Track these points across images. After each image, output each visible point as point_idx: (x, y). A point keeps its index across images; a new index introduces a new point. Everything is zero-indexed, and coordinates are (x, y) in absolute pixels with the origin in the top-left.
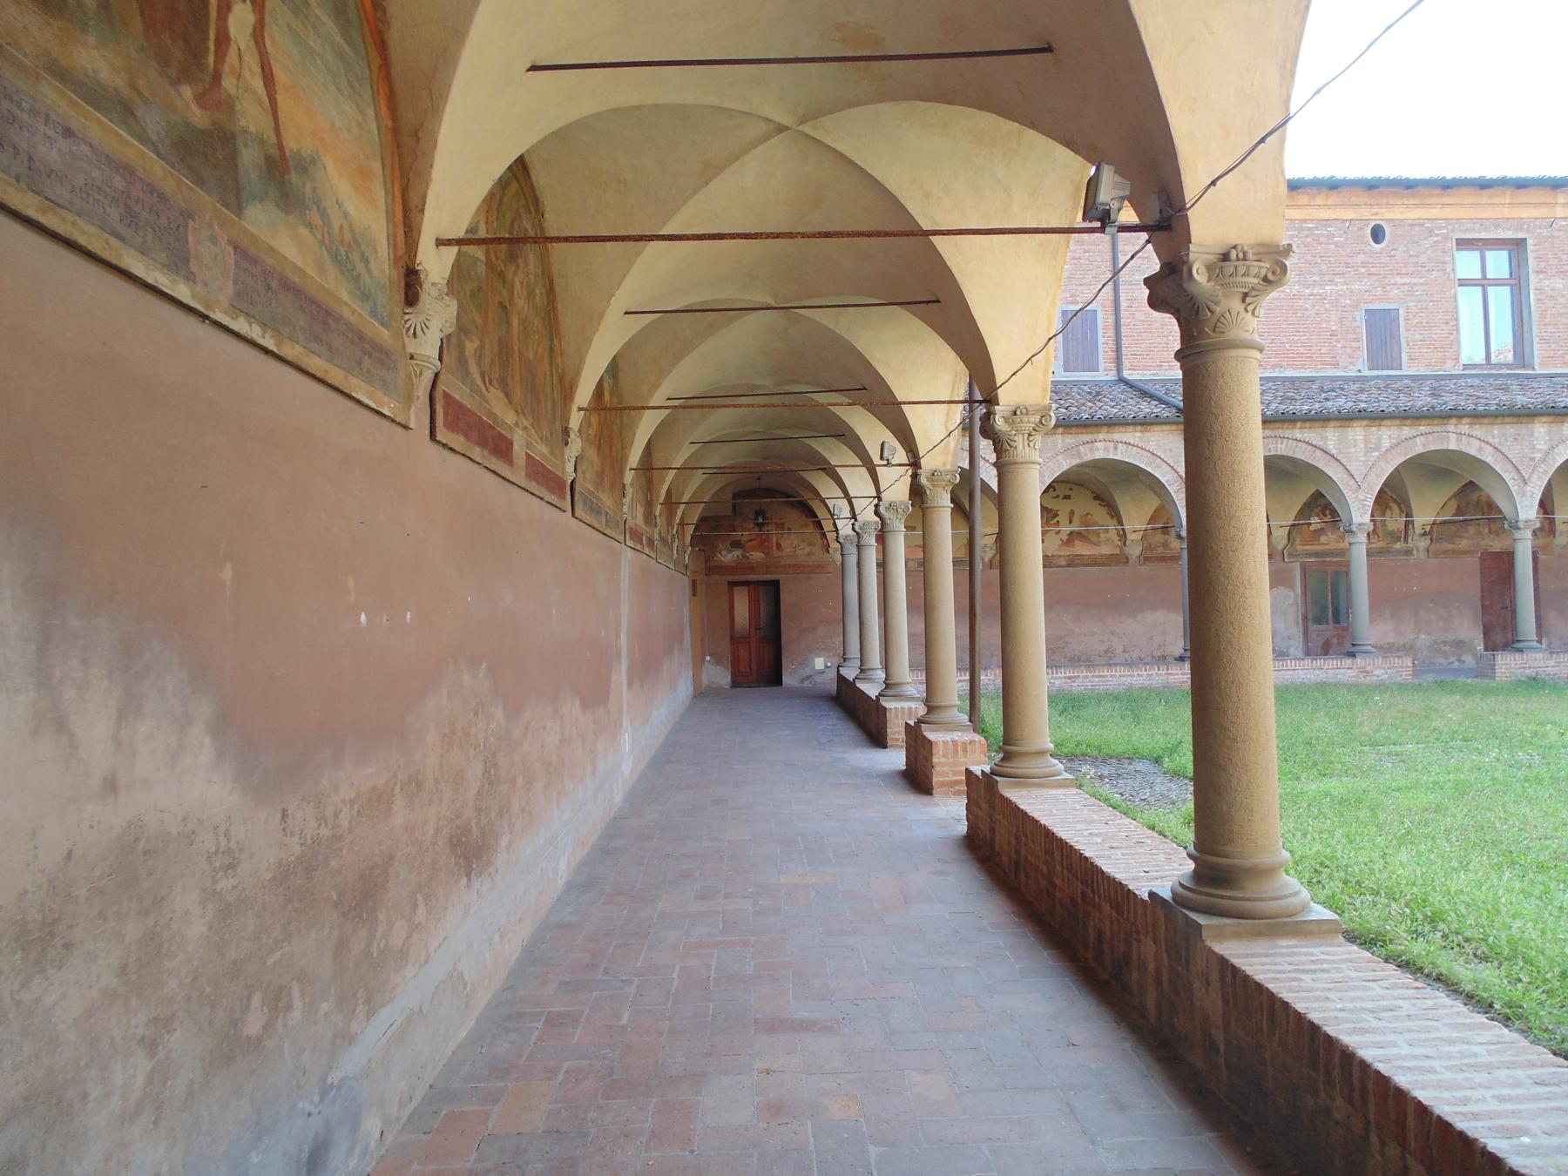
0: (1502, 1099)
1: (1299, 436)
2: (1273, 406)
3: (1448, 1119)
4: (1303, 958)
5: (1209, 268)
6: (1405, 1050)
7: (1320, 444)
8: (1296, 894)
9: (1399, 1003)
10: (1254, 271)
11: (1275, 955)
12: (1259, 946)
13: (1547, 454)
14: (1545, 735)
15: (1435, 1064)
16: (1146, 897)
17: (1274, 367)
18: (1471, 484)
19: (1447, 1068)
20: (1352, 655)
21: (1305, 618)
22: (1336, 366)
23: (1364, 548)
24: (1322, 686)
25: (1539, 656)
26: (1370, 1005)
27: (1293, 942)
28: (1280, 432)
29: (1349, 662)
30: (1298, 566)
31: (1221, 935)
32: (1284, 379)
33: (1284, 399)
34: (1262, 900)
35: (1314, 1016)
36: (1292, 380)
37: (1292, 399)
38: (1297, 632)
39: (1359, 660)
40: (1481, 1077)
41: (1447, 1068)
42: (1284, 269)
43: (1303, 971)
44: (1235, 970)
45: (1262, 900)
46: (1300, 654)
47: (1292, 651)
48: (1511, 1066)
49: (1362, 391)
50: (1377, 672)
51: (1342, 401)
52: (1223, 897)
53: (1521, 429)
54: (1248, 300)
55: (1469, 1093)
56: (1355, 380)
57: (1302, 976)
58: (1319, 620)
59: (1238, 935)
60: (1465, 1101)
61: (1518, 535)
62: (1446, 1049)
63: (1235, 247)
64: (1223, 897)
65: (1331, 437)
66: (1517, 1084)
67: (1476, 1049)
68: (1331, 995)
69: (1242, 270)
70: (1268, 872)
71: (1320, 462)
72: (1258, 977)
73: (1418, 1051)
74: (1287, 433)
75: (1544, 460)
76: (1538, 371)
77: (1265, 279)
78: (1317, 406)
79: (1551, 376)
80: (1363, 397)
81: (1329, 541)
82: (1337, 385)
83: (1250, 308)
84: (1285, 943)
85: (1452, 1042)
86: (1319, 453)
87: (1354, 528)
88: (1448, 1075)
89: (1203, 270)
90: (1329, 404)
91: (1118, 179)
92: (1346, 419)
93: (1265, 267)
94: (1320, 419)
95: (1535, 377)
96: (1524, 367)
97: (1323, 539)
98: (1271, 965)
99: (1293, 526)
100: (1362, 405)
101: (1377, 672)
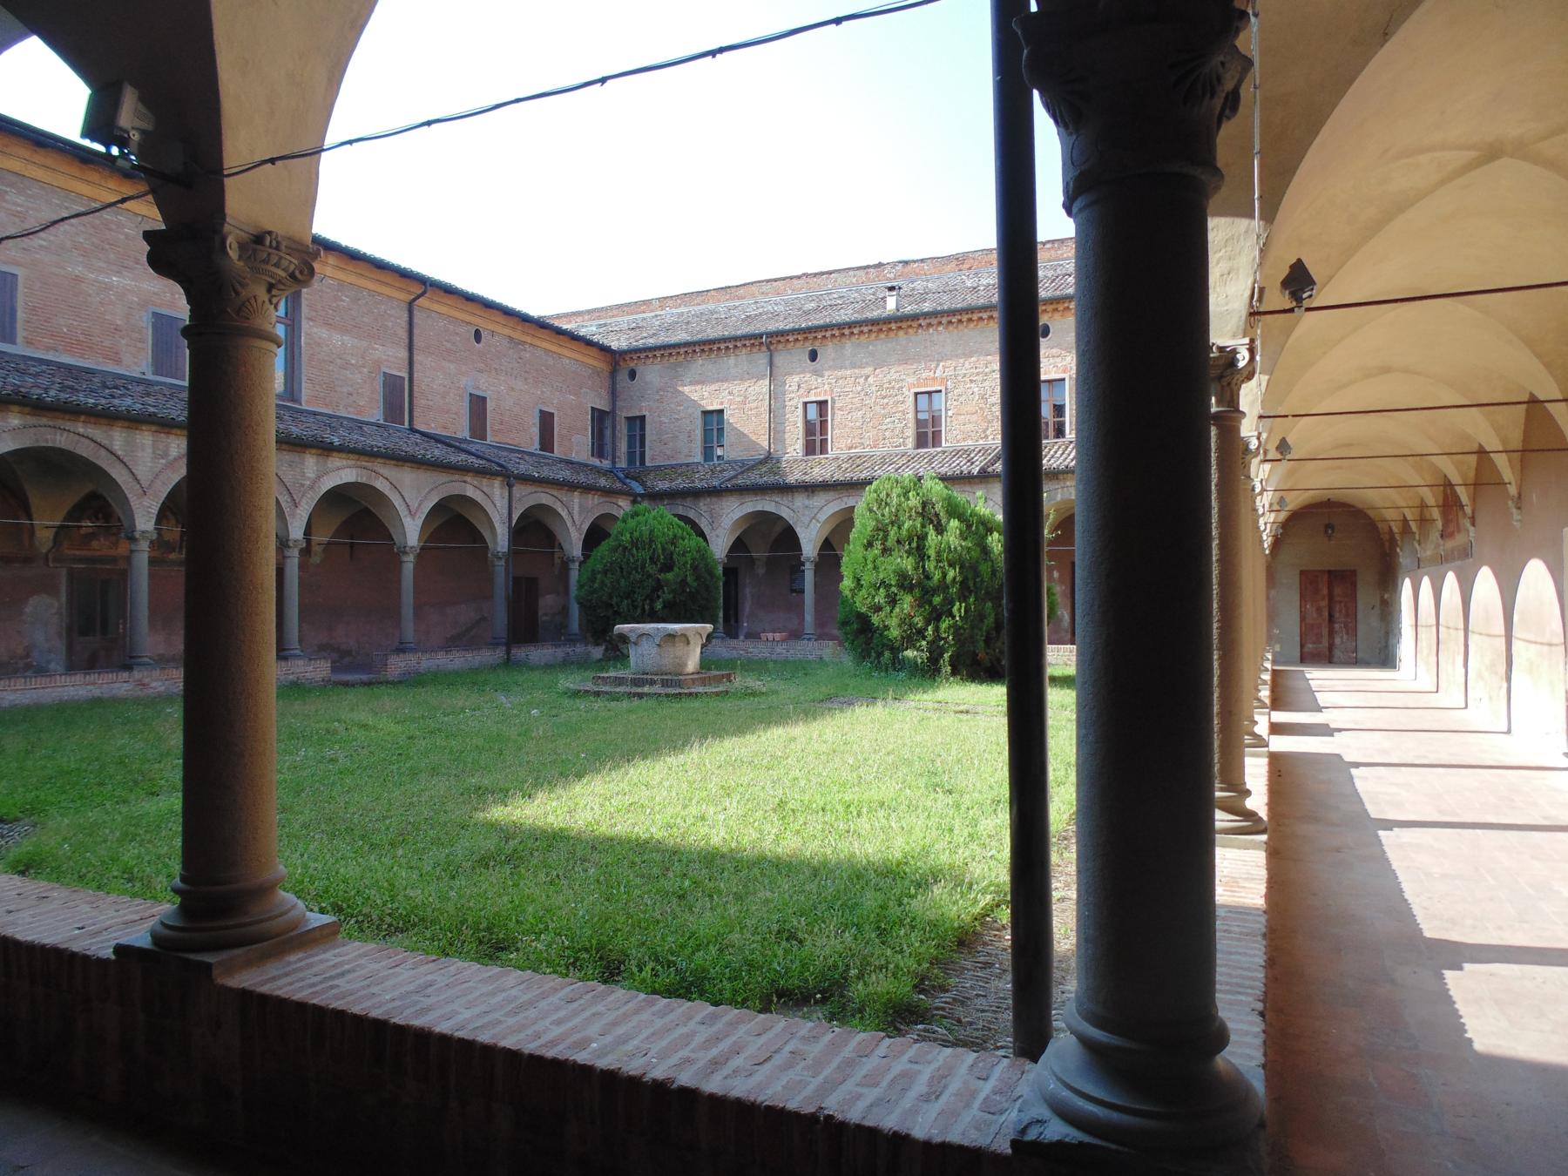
0: (558, 1023)
1: (81, 430)
2: (52, 393)
3: (538, 1053)
4: (322, 967)
5: (242, 247)
6: (467, 1014)
7: (105, 442)
8: (294, 907)
9: (429, 978)
10: (284, 263)
11: (295, 971)
12: (272, 969)
13: (314, 482)
14: (335, 732)
15: (497, 1015)
16: (108, 953)
17: (48, 349)
18: (367, 512)
19: (507, 1015)
20: (128, 668)
21: (70, 630)
22: (119, 362)
23: (146, 555)
24: (97, 702)
25: (301, 663)
26: (411, 987)
27: (300, 955)
28: (59, 423)
29: (125, 675)
30: (64, 572)
31: (231, 969)
32: (60, 366)
33: (63, 389)
34: (270, 919)
35: (375, 1013)
36: (69, 368)
37: (72, 388)
38: (60, 645)
39: (137, 674)
40: (532, 1013)
41: (507, 1015)
42: (312, 272)
43: (332, 978)
44: (264, 999)
45: (270, 919)
46: (61, 669)
47: (52, 666)
48: (544, 996)
49: (148, 395)
50: (154, 684)
51: (129, 401)
52: (227, 928)
53: (294, 457)
54: (274, 292)
55: (536, 1028)
56: (139, 382)
57: (336, 982)
58: (85, 631)
59: (248, 964)
60: (538, 1036)
61: (405, 559)
62: (493, 1001)
63: (270, 233)
64: (227, 928)
65: (118, 438)
66: (557, 1009)
67: (514, 992)
68: (375, 990)
69: (274, 259)
70: (266, 890)
71: (103, 461)
72: (297, 997)
73: (477, 1010)
74: (68, 425)
75: (311, 488)
76: (304, 407)
77: (292, 275)
78: (103, 401)
79: (315, 414)
80: (150, 400)
81: (101, 547)
82: (123, 383)
83: (274, 300)
84: (293, 958)
85: (493, 994)
86: (103, 452)
87: (137, 535)
88: (511, 1021)
89: (235, 245)
90: (116, 402)
91: (140, 106)
92: (135, 421)
93: (292, 262)
94: (109, 417)
95: (302, 412)
96: (293, 400)
97: (95, 544)
98: (304, 979)
99: (61, 527)
100: (152, 409)
101: (154, 684)
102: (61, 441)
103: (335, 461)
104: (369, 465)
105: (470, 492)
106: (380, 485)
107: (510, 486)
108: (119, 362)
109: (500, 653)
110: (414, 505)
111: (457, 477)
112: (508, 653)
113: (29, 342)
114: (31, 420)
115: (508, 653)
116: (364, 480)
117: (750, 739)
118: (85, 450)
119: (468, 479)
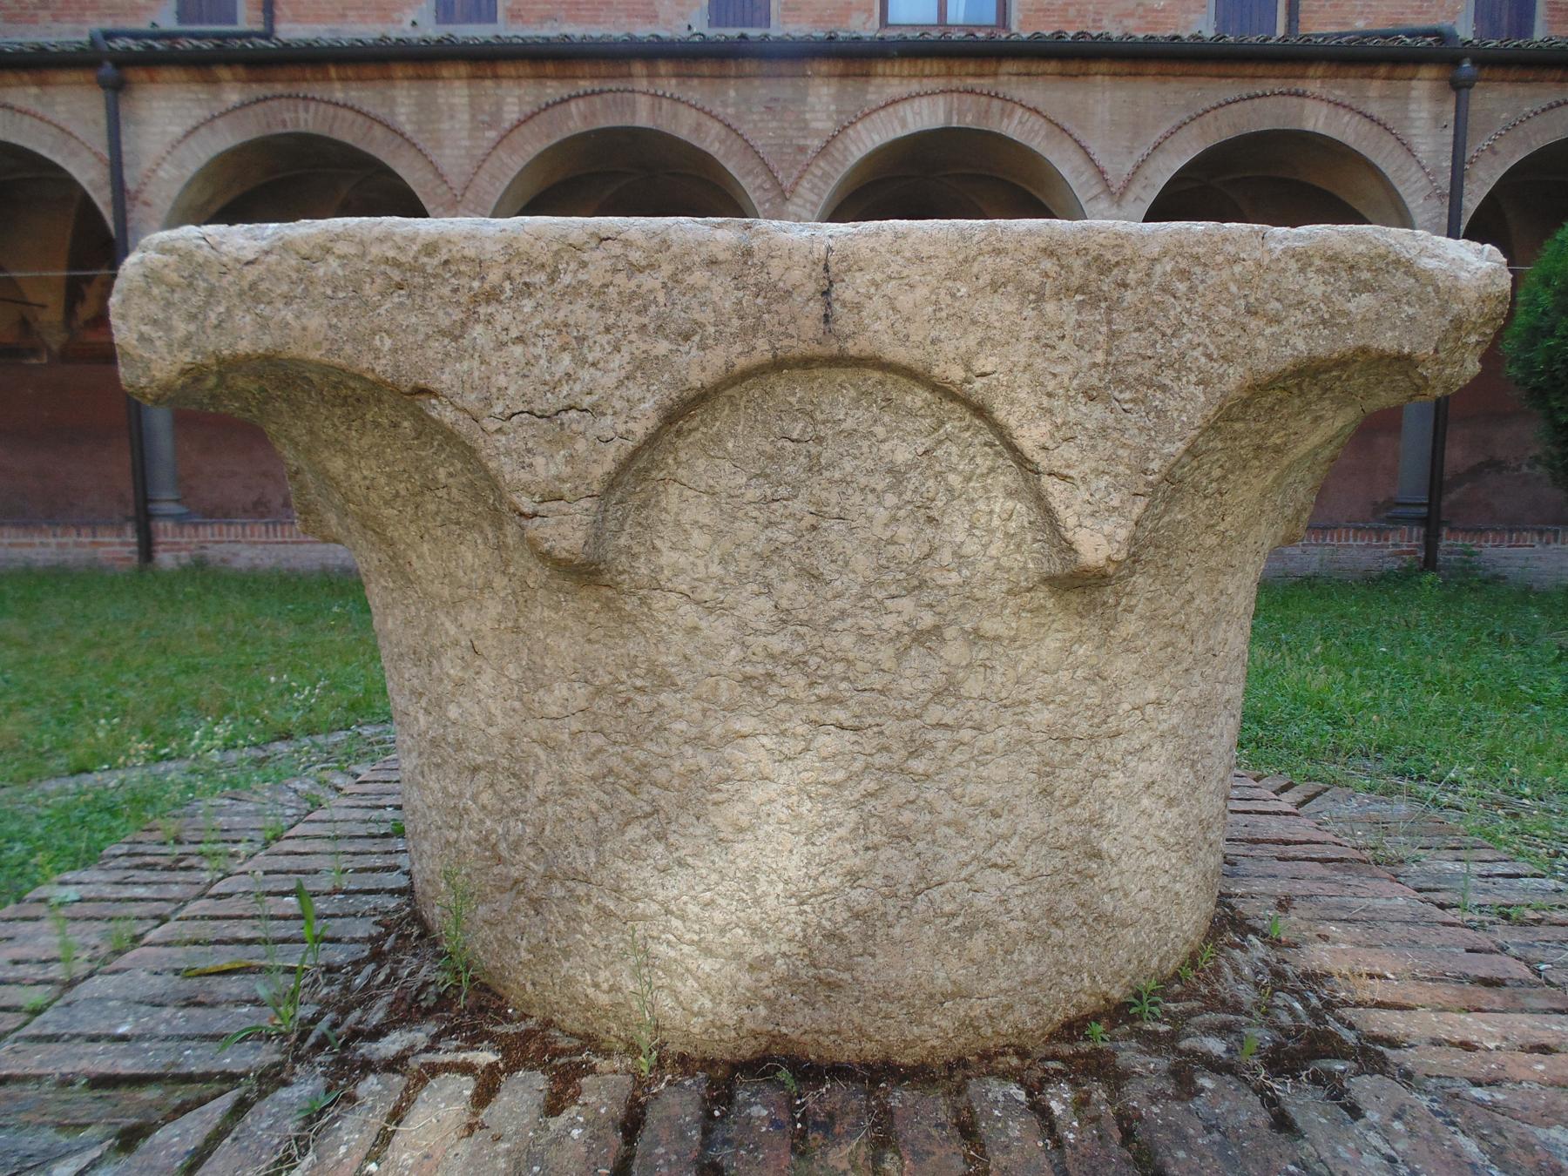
7: (381, 112)
17: (543, 19)
22: (653, 18)
28: (303, 89)
65: (402, 101)
74: (317, 90)
75: (823, 151)
86: (378, 131)
102: (306, 120)
103: (889, 84)
104: (986, 83)
105: (1317, 119)
106: (1014, 127)
107: (1459, 87)
108: (653, 18)
109: (1404, 543)
110: (1118, 168)
111: (1271, 85)
112: (1431, 544)
113: (515, 15)
114: (259, 90)
115: (1431, 544)
116: (969, 121)
117: (1228, 134)
118: (347, 132)
119: (1313, 87)
